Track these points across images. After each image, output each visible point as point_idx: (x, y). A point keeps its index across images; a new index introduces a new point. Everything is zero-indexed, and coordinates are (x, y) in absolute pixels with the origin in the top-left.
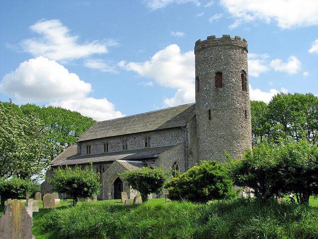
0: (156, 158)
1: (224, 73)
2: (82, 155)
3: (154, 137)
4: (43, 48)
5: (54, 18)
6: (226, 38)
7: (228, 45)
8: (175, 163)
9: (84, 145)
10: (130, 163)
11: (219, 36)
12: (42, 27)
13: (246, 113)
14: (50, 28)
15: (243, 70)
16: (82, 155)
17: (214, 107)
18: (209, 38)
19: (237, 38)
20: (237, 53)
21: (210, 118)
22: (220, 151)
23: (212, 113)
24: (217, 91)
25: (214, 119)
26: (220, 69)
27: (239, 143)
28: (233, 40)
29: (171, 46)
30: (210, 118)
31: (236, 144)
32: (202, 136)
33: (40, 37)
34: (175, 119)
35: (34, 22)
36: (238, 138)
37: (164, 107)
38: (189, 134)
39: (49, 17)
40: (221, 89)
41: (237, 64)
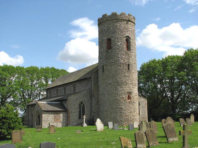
0: (66, 99)
1: (112, 39)
2: (48, 97)
3: (78, 85)
4: (79, 34)
5: (84, 17)
6: (114, 14)
7: (115, 19)
8: (82, 103)
9: (49, 91)
10: (48, 104)
11: (109, 14)
12: (77, 22)
13: (129, 66)
14: (82, 22)
15: (127, 36)
16: (48, 97)
17: (105, 63)
18: (103, 16)
19: (123, 14)
20: (123, 25)
21: (103, 71)
22: (109, 94)
23: (104, 67)
24: (107, 52)
25: (106, 72)
26: (110, 37)
27: (122, 88)
28: (119, 16)
29: (150, 25)
30: (103, 71)
31: (120, 89)
32: (100, 84)
33: (77, 28)
34: (88, 73)
35: (72, 21)
36: (122, 84)
37: (87, 66)
38: (92, 82)
39: (82, 16)
40: (110, 51)
41: (122, 32)
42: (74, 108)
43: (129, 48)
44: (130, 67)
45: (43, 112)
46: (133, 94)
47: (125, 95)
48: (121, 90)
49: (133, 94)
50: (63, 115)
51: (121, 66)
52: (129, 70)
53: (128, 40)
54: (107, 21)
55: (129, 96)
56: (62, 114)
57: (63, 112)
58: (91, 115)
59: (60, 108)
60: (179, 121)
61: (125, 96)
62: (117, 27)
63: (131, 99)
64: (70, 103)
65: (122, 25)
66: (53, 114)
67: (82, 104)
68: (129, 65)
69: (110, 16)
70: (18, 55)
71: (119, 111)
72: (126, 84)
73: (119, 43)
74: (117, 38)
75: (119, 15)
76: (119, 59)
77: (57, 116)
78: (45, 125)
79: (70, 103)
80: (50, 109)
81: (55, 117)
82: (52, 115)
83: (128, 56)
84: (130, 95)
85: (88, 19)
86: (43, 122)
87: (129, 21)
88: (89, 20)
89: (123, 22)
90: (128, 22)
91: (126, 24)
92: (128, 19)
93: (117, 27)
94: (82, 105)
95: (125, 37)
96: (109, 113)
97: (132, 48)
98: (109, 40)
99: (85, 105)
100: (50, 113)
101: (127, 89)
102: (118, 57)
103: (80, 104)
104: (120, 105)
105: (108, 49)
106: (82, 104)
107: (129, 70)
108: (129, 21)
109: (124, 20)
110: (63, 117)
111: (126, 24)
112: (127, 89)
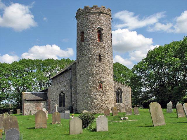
1: (85, 32)
6: (86, 8)
8: (62, 92)
11: (82, 8)
12: (117, 15)
14: (121, 15)
15: (99, 28)
20: (95, 17)
27: (93, 78)
28: (90, 9)
31: (91, 79)
39: (122, 9)
40: (83, 43)
42: (54, 97)
43: (100, 39)
44: (101, 57)
45: (24, 102)
46: (105, 84)
47: (96, 84)
48: (92, 80)
49: (105, 84)
50: (44, 104)
51: (92, 57)
52: (100, 60)
53: (100, 31)
54: (81, 15)
55: (100, 85)
56: (43, 102)
57: (43, 101)
58: (71, 104)
59: (41, 97)
60: (149, 108)
61: (97, 86)
62: (88, 20)
63: (102, 88)
64: (51, 93)
65: (94, 18)
66: (34, 103)
67: (62, 93)
68: (100, 56)
69: (83, 10)
70: (68, 48)
71: (91, 99)
72: (97, 73)
73: (91, 36)
74: (89, 30)
75: (91, 8)
76: (90, 51)
77: (38, 104)
78: (26, 113)
79: (51, 93)
80: (31, 99)
81: (36, 106)
82: (33, 104)
83: (100, 47)
84: (101, 85)
85: (127, 12)
86: (24, 110)
87: (101, 13)
88: (129, 12)
89: (95, 15)
90: (100, 15)
91: (98, 16)
92: (100, 11)
93: (88, 20)
94: (62, 95)
95: (97, 29)
96: (82, 101)
97: (86, 39)
98: (83, 33)
99: (65, 94)
100: (31, 102)
101: (98, 79)
102: (89, 49)
103: (60, 94)
104: (91, 94)
105: (82, 41)
106: (62, 93)
107: (100, 60)
108: (101, 13)
109: (95, 13)
110: (44, 105)
111: (98, 16)
112: (98, 79)
